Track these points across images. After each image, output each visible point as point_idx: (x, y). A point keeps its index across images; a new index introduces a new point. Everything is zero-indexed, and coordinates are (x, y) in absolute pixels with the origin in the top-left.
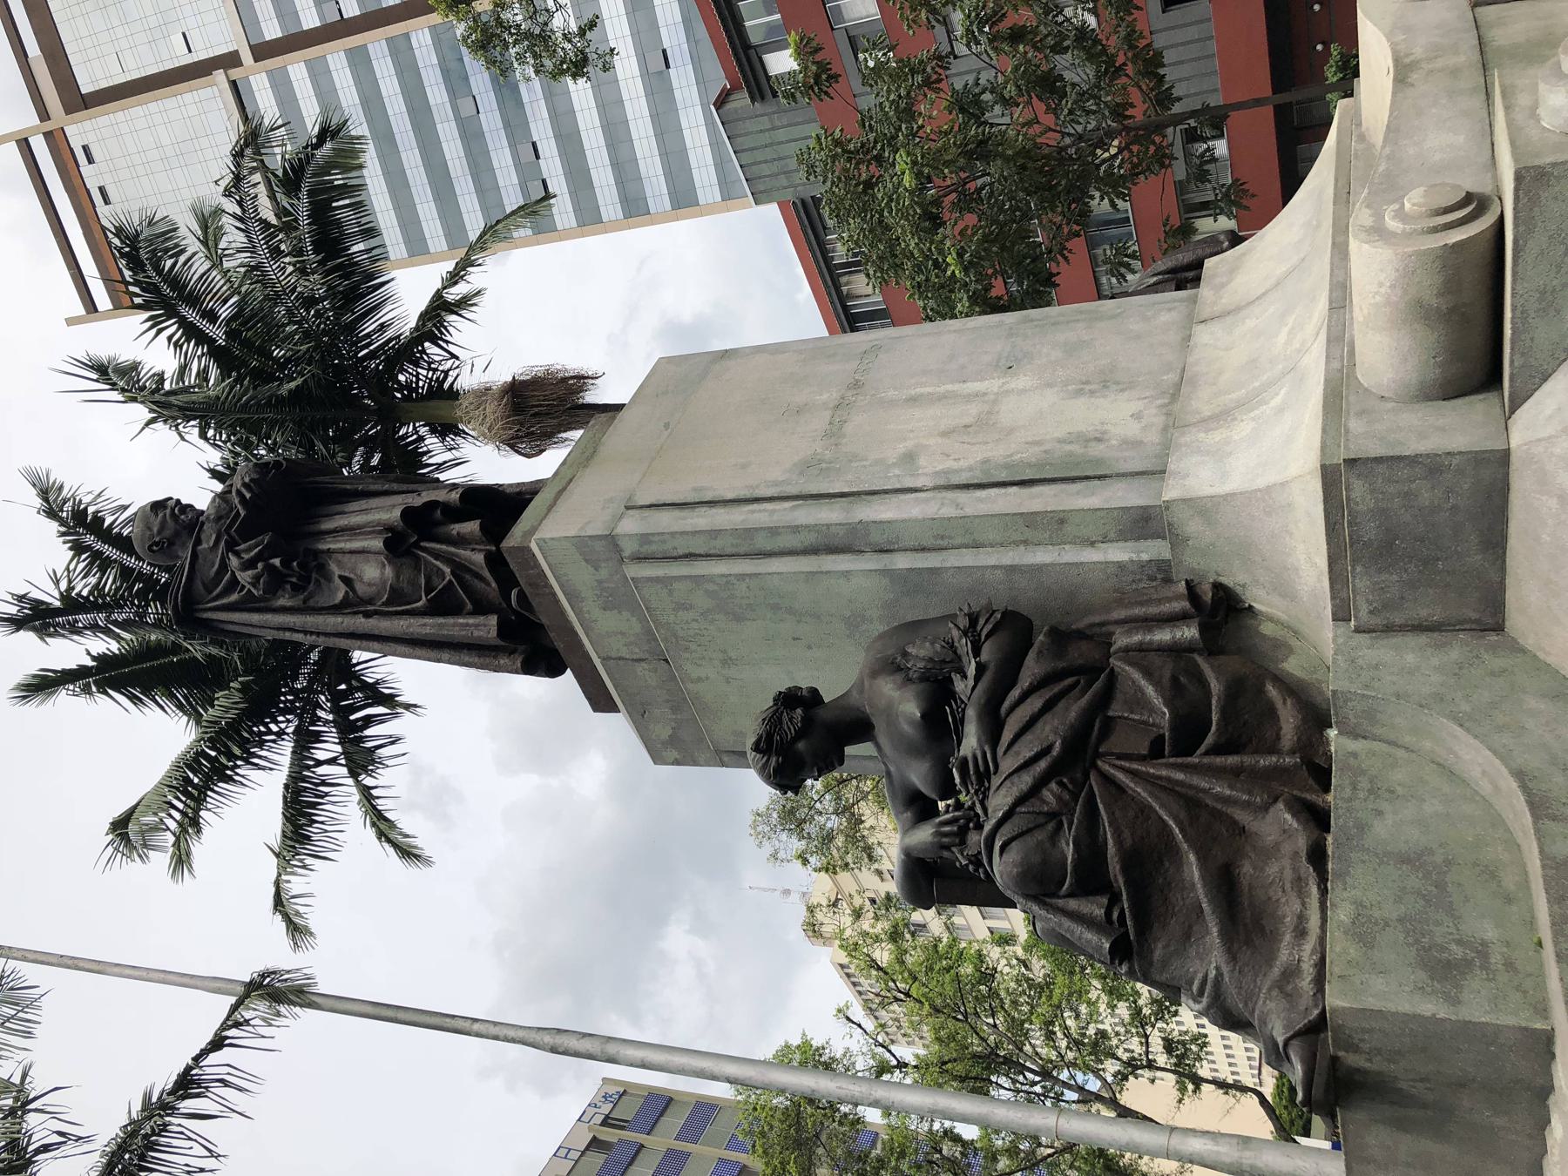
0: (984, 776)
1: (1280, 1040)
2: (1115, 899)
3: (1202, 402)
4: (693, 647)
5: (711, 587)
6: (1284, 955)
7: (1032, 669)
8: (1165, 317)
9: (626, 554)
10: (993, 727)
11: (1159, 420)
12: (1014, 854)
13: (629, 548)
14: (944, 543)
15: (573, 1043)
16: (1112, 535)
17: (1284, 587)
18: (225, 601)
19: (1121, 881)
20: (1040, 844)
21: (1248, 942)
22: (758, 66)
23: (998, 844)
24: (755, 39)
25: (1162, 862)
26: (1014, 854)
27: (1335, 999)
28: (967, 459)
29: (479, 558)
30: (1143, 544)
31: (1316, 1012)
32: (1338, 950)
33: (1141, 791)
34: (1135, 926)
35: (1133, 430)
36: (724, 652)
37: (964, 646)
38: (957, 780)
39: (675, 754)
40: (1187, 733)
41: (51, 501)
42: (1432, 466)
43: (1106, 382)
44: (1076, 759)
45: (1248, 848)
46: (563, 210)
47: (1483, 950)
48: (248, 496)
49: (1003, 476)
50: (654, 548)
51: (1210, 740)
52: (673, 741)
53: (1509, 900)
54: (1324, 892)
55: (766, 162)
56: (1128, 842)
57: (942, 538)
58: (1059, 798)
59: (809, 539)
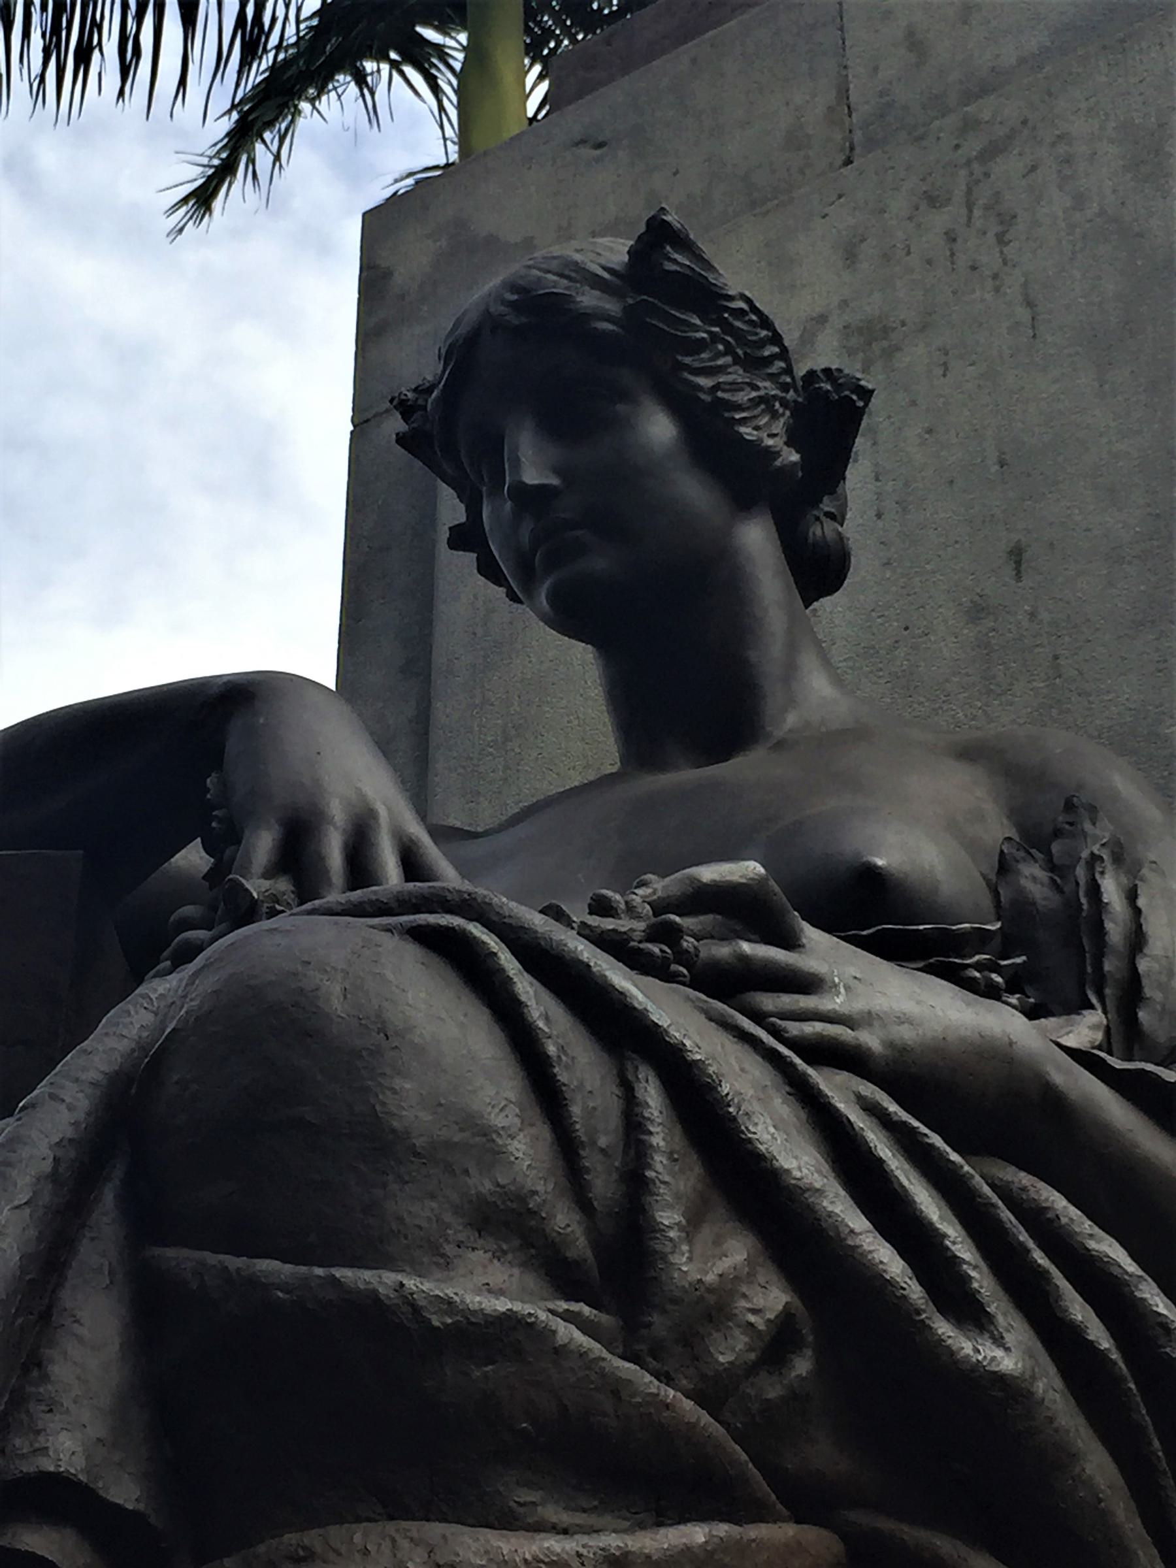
20: (486, 1146)
38: (709, 873)
58: (714, 1308)
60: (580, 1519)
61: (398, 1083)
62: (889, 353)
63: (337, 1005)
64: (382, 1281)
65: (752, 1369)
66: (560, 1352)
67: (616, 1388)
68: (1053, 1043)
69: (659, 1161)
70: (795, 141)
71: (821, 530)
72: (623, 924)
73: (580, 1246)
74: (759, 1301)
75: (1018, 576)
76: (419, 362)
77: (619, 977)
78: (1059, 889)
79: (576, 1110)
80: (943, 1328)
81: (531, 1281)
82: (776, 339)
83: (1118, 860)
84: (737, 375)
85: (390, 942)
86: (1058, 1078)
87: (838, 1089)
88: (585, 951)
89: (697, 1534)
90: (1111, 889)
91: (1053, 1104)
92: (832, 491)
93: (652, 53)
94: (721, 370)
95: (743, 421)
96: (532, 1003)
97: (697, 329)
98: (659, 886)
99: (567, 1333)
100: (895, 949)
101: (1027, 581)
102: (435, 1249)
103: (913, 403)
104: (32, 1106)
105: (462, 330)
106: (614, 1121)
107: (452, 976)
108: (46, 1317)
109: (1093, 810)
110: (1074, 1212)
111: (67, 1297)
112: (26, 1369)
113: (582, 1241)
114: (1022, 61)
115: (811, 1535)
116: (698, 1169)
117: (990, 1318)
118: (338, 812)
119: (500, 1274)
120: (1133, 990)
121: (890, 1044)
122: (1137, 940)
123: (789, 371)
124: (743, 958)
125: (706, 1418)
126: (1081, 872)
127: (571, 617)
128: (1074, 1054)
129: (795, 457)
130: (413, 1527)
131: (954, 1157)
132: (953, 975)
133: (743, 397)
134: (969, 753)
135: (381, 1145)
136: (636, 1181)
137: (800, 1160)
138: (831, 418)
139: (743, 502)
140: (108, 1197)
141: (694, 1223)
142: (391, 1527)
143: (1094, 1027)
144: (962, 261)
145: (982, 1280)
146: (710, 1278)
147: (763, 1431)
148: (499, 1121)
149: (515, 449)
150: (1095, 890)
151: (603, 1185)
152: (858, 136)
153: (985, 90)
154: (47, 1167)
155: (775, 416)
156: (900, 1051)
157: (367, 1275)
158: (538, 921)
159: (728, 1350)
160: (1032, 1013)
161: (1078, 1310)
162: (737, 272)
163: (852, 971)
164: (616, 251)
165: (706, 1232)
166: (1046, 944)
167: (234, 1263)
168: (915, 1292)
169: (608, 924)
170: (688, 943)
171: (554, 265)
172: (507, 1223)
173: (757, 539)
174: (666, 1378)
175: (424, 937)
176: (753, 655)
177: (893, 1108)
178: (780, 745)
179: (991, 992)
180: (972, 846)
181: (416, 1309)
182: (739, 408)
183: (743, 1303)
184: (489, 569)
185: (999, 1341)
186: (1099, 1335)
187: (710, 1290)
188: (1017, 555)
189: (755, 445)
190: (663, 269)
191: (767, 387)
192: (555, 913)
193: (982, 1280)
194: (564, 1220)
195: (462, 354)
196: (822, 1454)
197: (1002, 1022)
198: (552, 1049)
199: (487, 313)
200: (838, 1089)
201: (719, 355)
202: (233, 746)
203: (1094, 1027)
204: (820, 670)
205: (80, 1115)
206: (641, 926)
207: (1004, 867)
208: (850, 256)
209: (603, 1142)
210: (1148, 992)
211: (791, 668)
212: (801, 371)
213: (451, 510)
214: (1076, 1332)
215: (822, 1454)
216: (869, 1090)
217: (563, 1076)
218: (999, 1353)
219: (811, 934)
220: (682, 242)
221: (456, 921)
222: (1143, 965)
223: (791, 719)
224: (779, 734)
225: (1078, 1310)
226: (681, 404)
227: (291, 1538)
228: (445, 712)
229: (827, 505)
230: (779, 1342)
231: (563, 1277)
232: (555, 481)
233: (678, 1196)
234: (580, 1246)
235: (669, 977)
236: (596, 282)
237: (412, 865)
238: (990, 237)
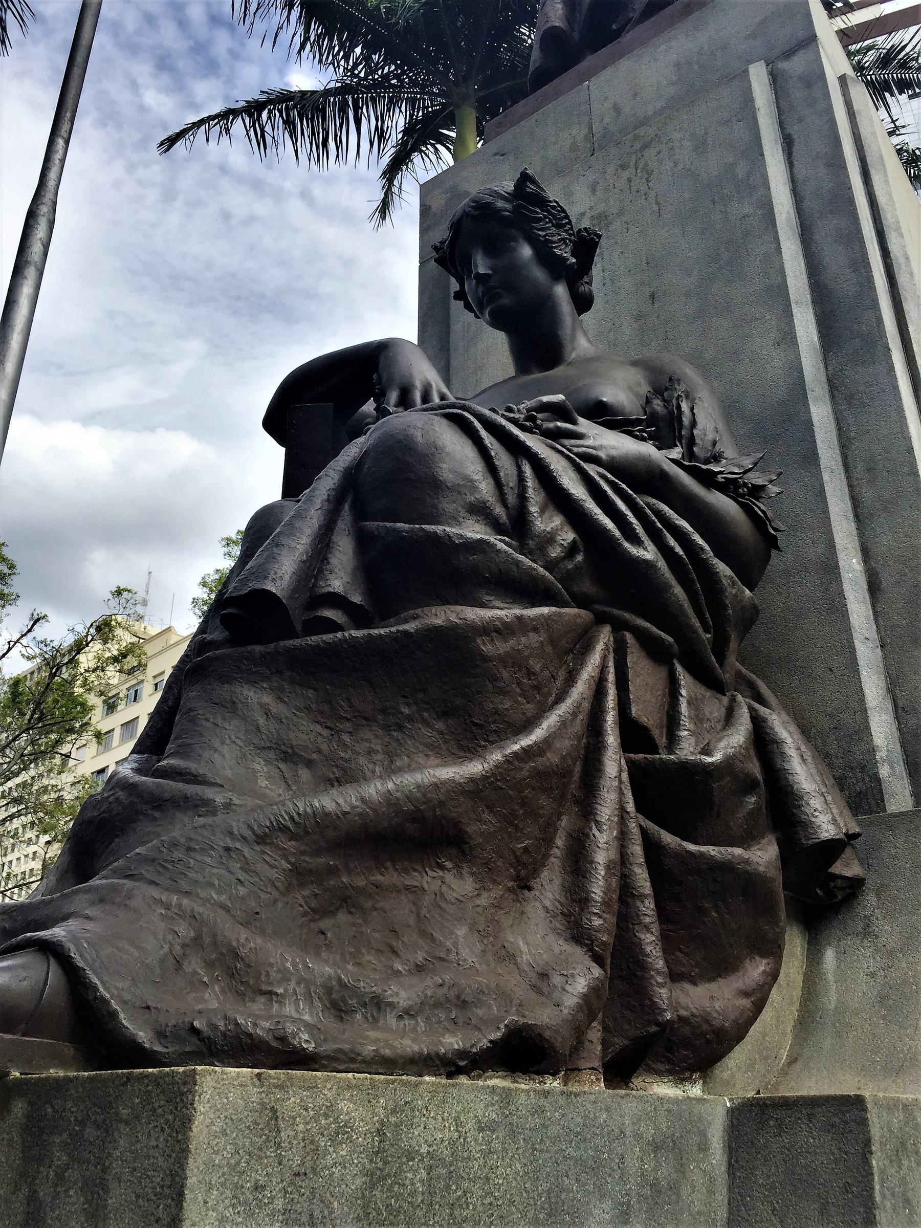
1: (57, 932)
2: (359, 617)
6: (281, 956)
9: (783, 65)
13: (796, 65)
14: (859, 469)
15: (40, 232)
16: (912, 722)
19: (411, 627)
20: (472, 486)
21: (299, 875)
25: (444, 715)
27: (222, 1093)
30: (900, 769)
31: (144, 1037)
32: (345, 1106)
33: (581, 689)
34: (315, 648)
36: (620, 214)
38: (545, 399)
41: (138, 717)
45: (497, 891)
51: (669, 839)
56: (487, 648)
57: (870, 470)
58: (550, 539)
60: (506, 605)
61: (441, 465)
62: (607, 226)
63: (419, 439)
64: (438, 529)
65: (563, 558)
66: (499, 551)
67: (517, 563)
68: (665, 458)
69: (530, 491)
70: (574, 148)
71: (584, 288)
72: (517, 416)
73: (504, 518)
74: (564, 537)
75: (653, 303)
76: (442, 233)
77: (516, 431)
78: (667, 408)
79: (502, 474)
80: (626, 545)
81: (488, 530)
82: (567, 217)
83: (687, 397)
84: (553, 230)
85: (437, 418)
86: (666, 467)
87: (592, 470)
88: (504, 422)
89: (545, 610)
90: (685, 406)
91: (664, 476)
92: (587, 274)
93: (522, 118)
94: (548, 228)
95: (555, 247)
96: (486, 438)
97: (538, 213)
98: (529, 404)
99: (501, 546)
100: (612, 425)
101: (656, 305)
102: (455, 519)
103: (616, 243)
104: (319, 478)
105: (456, 217)
106: (515, 478)
107: (458, 430)
108: (328, 545)
109: (679, 380)
110: (671, 512)
111: (335, 538)
112: (322, 561)
113: (505, 518)
114: (655, 112)
115: (583, 612)
116: (543, 494)
117: (643, 542)
118: (418, 385)
119: (477, 527)
120: (692, 441)
121: (608, 456)
122: (694, 424)
123: (572, 229)
124: (558, 428)
125: (547, 574)
126: (674, 401)
127: (497, 322)
128: (674, 461)
129: (574, 260)
130: (452, 607)
131: (630, 492)
132: (630, 434)
133: (555, 238)
134: (635, 364)
135: (436, 485)
136: (522, 498)
137: (578, 491)
138: (587, 246)
139: (556, 278)
140: (347, 507)
141: (542, 511)
142: (444, 607)
143: (679, 453)
144: (634, 189)
145: (639, 530)
146: (548, 529)
147: (567, 579)
148: (476, 478)
149: (476, 261)
150: (679, 407)
151: (511, 499)
152: (596, 145)
153: (642, 124)
154: (326, 497)
155: (567, 245)
156: (612, 459)
157: (433, 527)
158: (487, 412)
159: (555, 552)
160: (659, 449)
161: (672, 542)
162: (553, 193)
163: (596, 432)
164: (509, 186)
165: (546, 515)
166: (665, 426)
167: (388, 525)
168: (617, 533)
169: (512, 415)
170: (539, 422)
171: (487, 192)
172: (480, 511)
173: (561, 291)
174: (535, 562)
175: (446, 416)
176: (560, 333)
177: (609, 476)
178: (570, 364)
179: (643, 439)
180: (637, 395)
181: (449, 537)
182: (554, 242)
183: (559, 538)
184: (468, 307)
185: (645, 549)
186: (679, 550)
187: (548, 533)
188: (652, 296)
189: (560, 256)
190: (527, 192)
191: (564, 235)
192: (493, 410)
193: (639, 530)
194: (499, 510)
195: (457, 227)
196: (586, 587)
197: (647, 449)
198: (493, 454)
199: (464, 212)
200: (592, 470)
201: (547, 223)
202: (381, 364)
203: (679, 453)
204: (583, 338)
205: (336, 481)
206: (523, 416)
207: (648, 401)
208: (594, 191)
209: (511, 485)
210: (697, 441)
211: (574, 337)
212: (575, 230)
213: (454, 286)
214: (672, 549)
215: (586, 587)
216: (601, 470)
217: (497, 463)
218: (646, 553)
219: (581, 420)
220: (533, 182)
221: (459, 411)
222: (695, 432)
223: (574, 355)
224: (569, 360)
225: (672, 542)
226: (533, 242)
227: (412, 612)
228: (454, 363)
229: (586, 279)
230: (572, 550)
231: (497, 527)
232: (490, 272)
233: (537, 502)
234: (504, 518)
235: (532, 433)
236: (503, 198)
237: (443, 397)
238: (644, 180)
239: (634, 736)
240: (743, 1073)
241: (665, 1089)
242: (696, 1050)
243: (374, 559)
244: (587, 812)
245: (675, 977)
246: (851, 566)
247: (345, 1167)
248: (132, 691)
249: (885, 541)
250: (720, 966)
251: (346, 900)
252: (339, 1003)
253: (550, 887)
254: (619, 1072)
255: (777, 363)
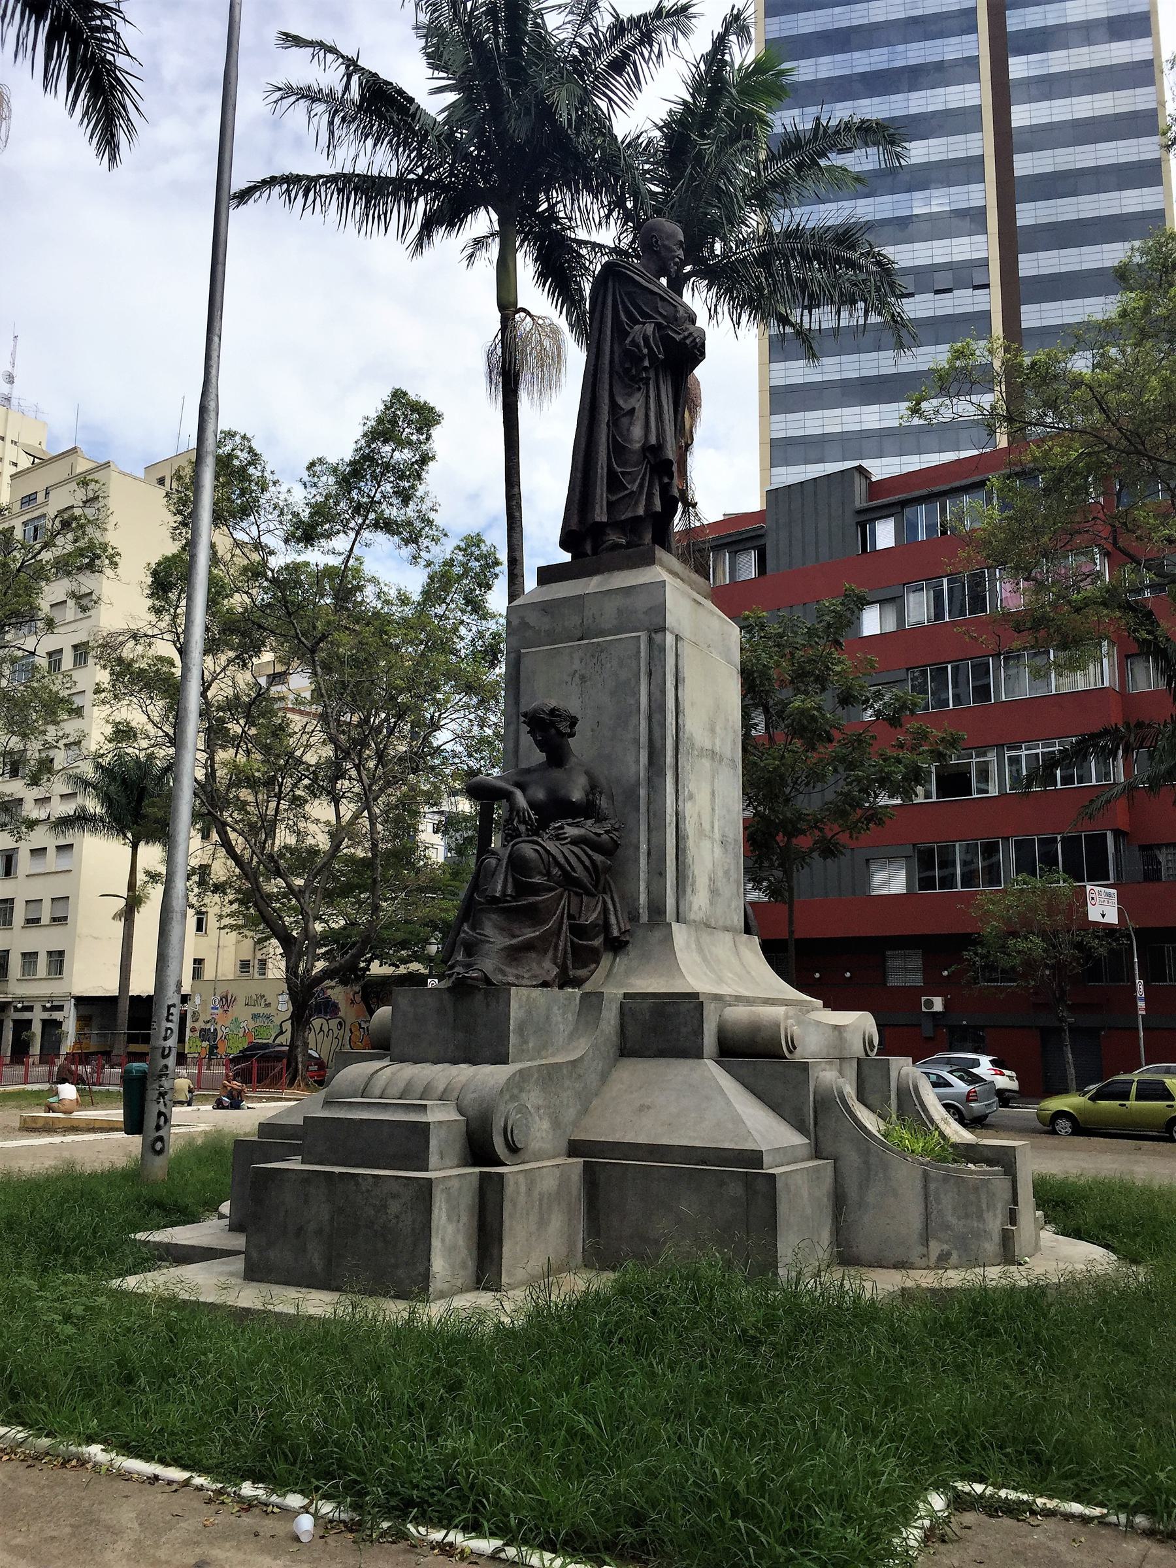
0: (558, 838)
3: (706, 938)
4: (595, 661)
5: (633, 682)
6: (508, 970)
7: (598, 858)
8: (736, 918)
10: (576, 841)
11: (697, 919)
12: (533, 855)
13: (657, 637)
17: (629, 972)
18: (622, 314)
22: (885, 512)
23: (538, 848)
24: (908, 511)
26: (533, 855)
27: (513, 989)
28: (690, 828)
29: (641, 511)
35: (695, 907)
37: (608, 827)
39: (515, 622)
40: (579, 931)
42: (699, 1032)
43: (714, 892)
44: (568, 881)
46: (797, 372)
47: (526, 1042)
48: (688, 342)
49: (681, 846)
50: (656, 653)
52: (524, 625)
53: (539, 1053)
54: (534, 986)
55: (803, 505)
59: (658, 744)
239: (571, 917)
240: (588, 987)
241: (570, 990)
242: (577, 983)
243: (517, 884)
244: (559, 938)
245: (574, 968)
246: (644, 847)
247: (524, 998)
248: (31, 527)
249: (653, 840)
250: (585, 966)
251: (516, 959)
252: (517, 977)
253: (550, 954)
254: (561, 987)
255: (633, 769)
